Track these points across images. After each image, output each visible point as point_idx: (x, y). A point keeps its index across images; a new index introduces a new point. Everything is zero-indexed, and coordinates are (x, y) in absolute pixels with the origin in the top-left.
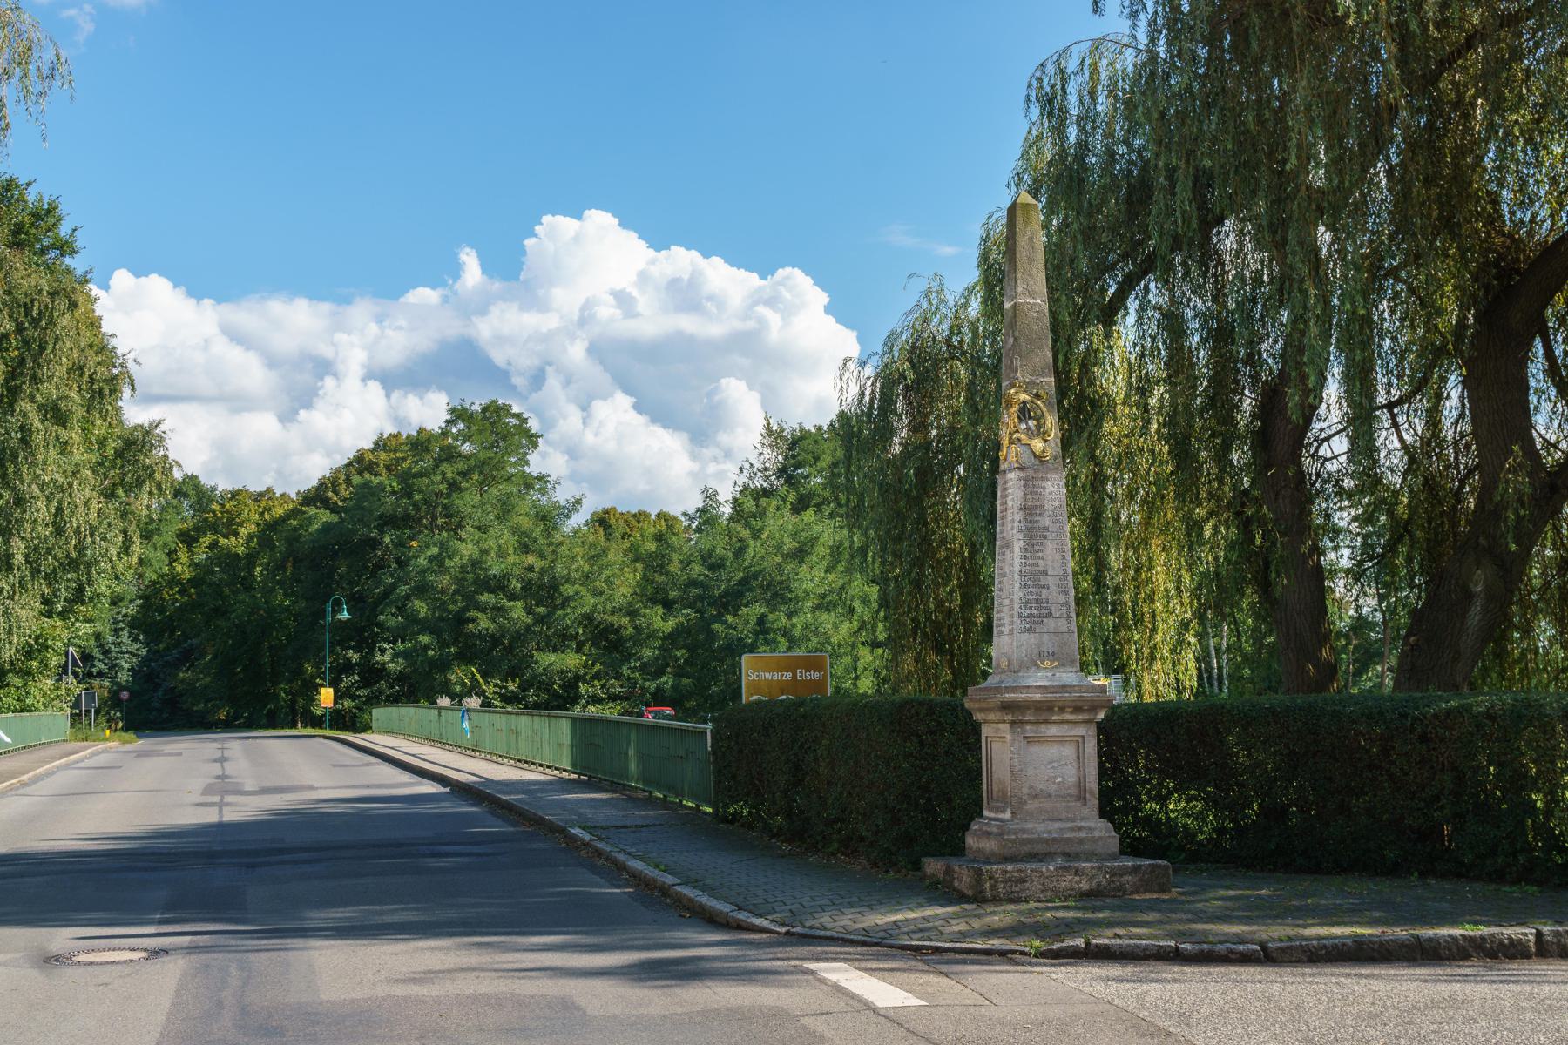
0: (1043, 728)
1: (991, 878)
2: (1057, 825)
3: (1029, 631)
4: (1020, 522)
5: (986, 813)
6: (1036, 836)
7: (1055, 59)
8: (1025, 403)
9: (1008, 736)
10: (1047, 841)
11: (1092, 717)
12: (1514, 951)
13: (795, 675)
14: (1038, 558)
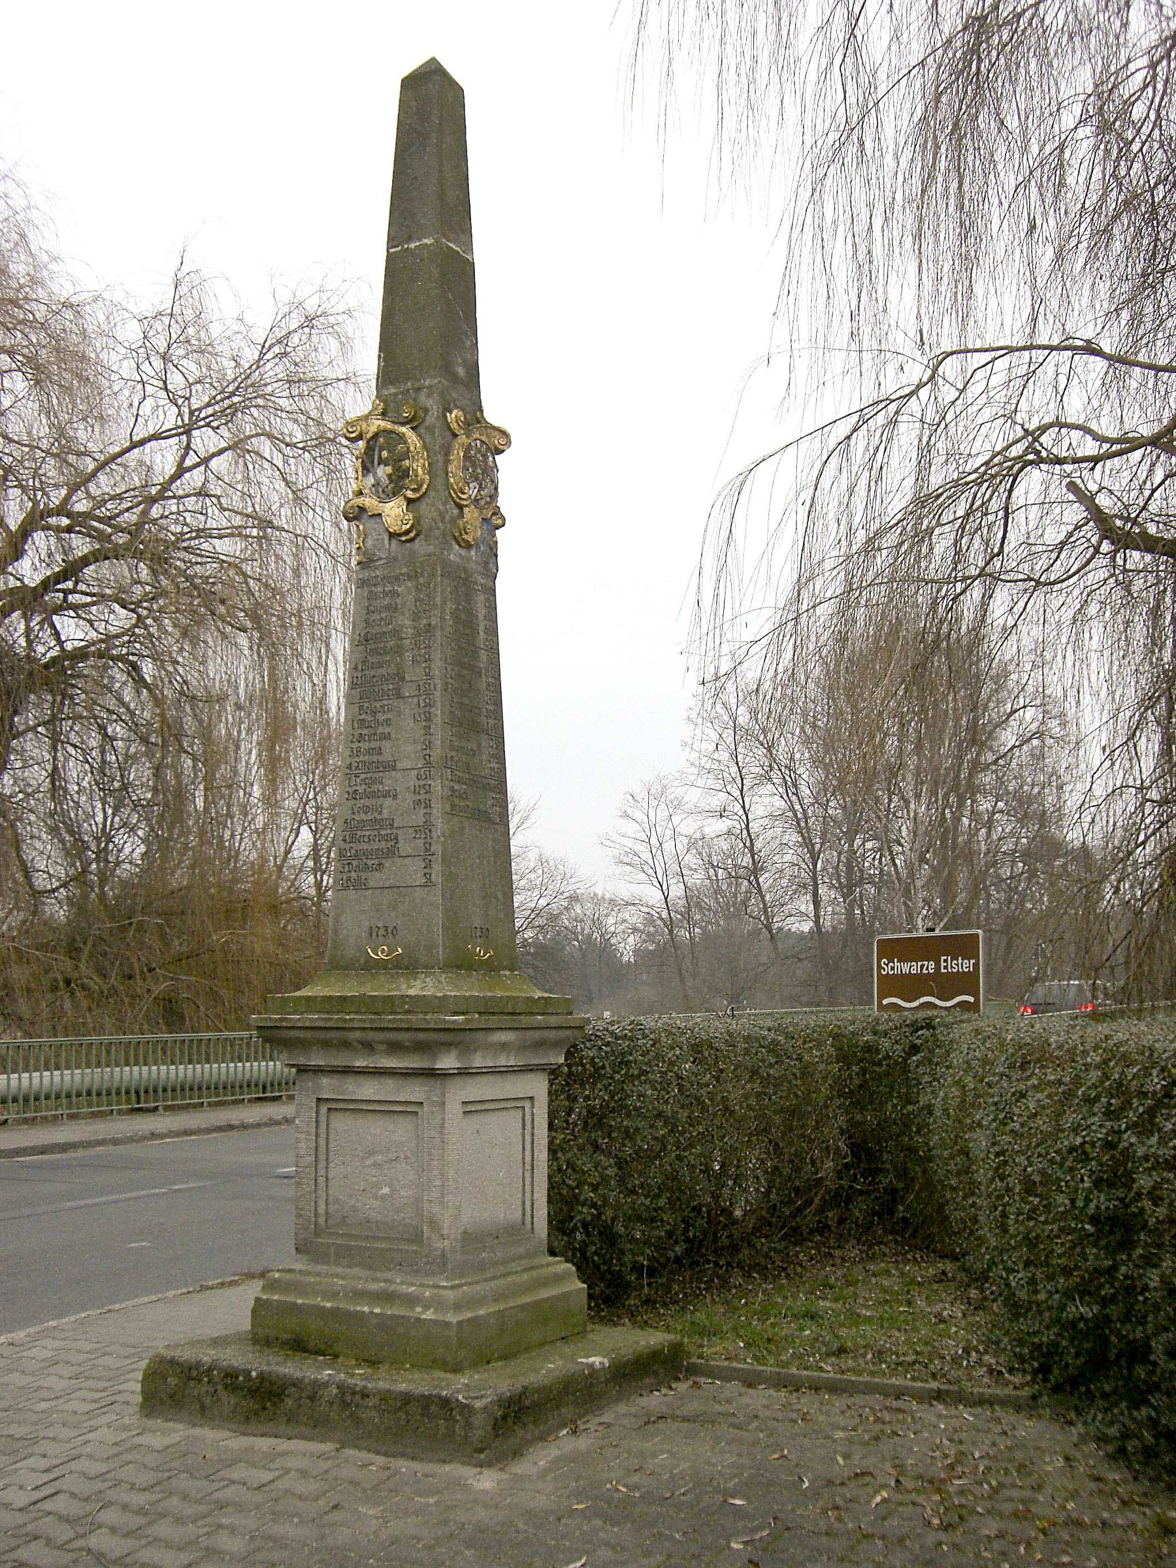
11: (426, 1065)
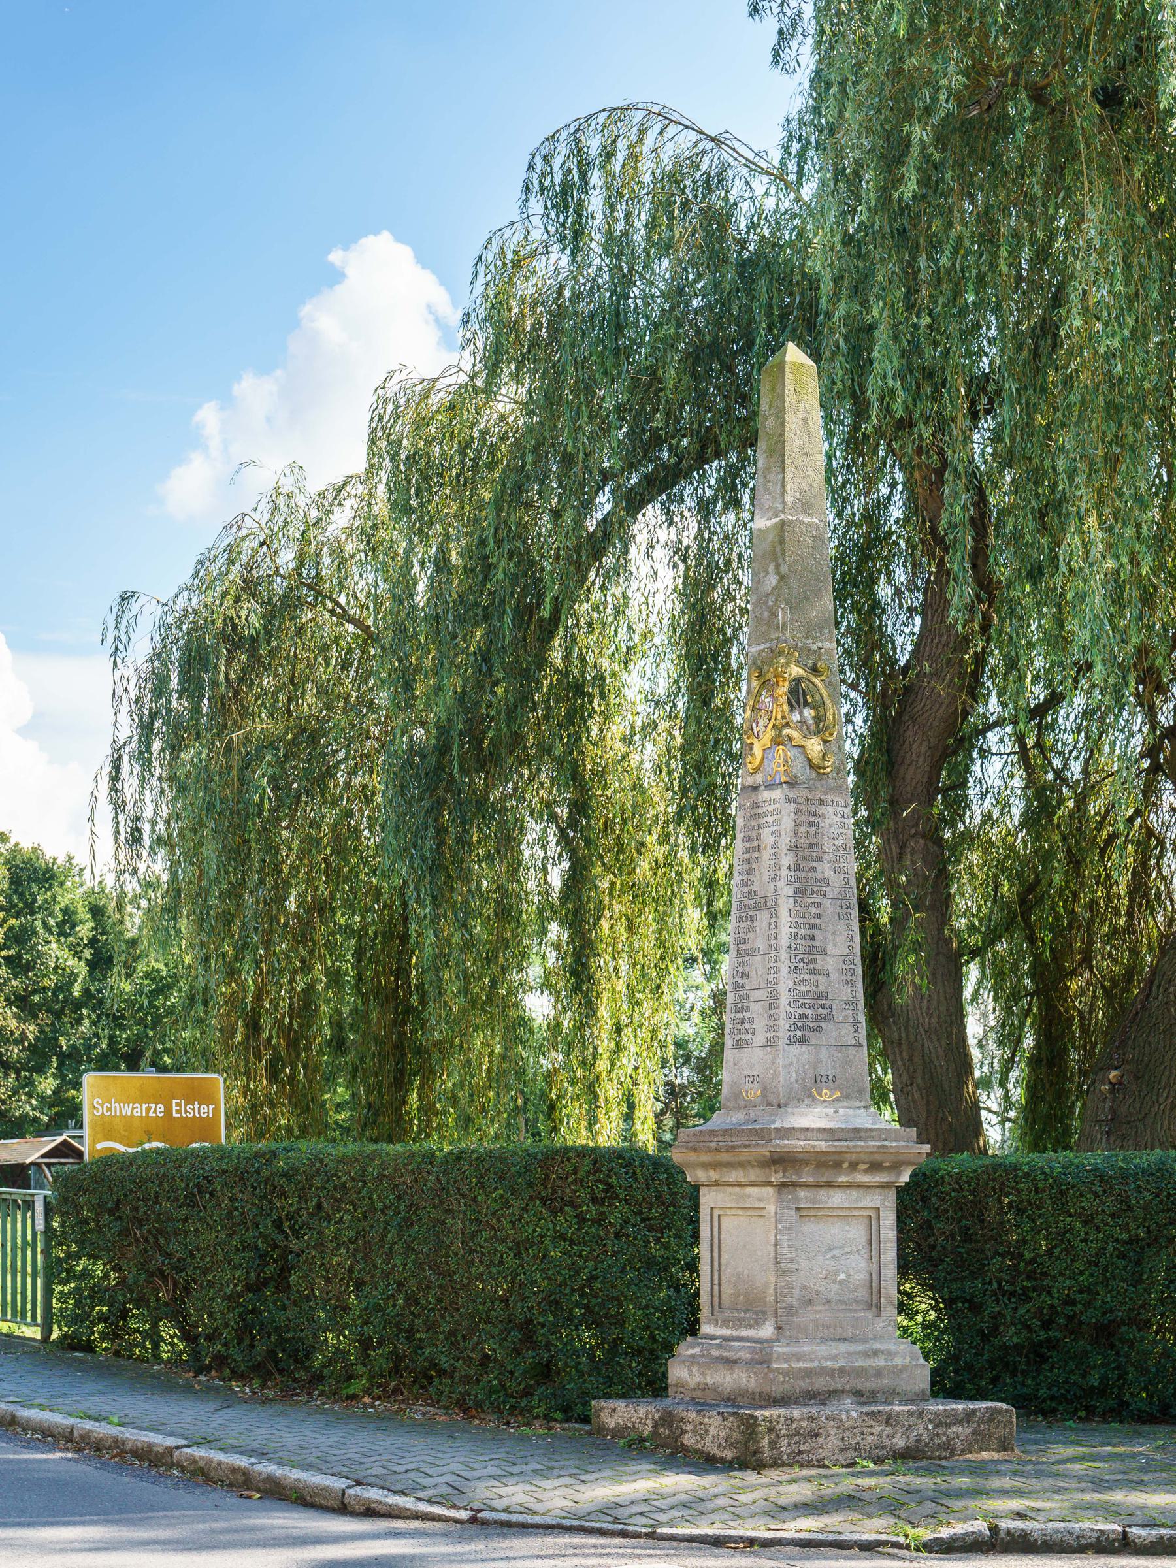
0: (822, 1194)
1: (770, 1430)
2: (843, 1347)
3: (802, 1041)
4: (789, 868)
5: (706, 1329)
6: (816, 1364)
7: (572, 130)
8: (798, 680)
9: (771, 1208)
10: (831, 1373)
12: (639, 1556)
13: (168, 1110)
14: (814, 926)
